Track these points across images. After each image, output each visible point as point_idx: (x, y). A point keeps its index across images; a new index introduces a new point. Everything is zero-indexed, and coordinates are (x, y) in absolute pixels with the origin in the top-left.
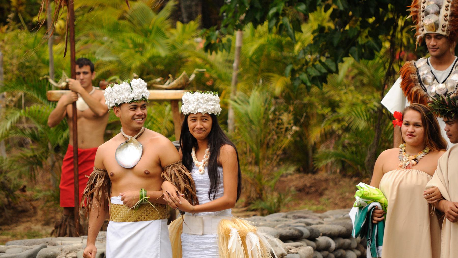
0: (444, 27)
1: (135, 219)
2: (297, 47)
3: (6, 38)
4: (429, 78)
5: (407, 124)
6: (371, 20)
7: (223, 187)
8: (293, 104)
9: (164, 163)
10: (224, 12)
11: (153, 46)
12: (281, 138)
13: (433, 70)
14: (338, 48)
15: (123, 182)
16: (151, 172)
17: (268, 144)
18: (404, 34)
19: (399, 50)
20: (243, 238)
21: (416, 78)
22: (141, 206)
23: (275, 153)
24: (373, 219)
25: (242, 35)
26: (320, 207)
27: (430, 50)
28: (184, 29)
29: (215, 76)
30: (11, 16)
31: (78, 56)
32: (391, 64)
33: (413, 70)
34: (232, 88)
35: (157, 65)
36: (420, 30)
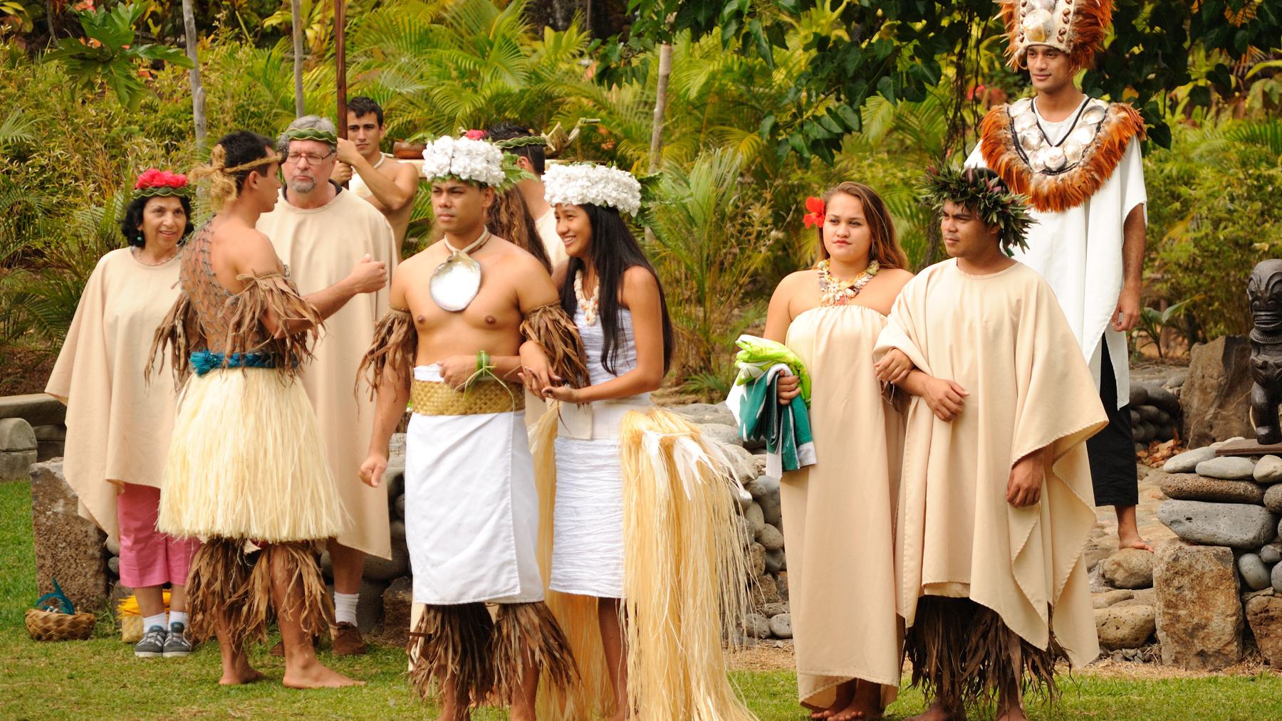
0: (1062, 34)
1: (462, 409)
2: (779, 76)
3: (210, 58)
4: (1033, 137)
5: (836, 221)
6: (919, 26)
7: (634, 348)
8: (772, 185)
9: (527, 305)
10: (636, 9)
11: (495, 74)
12: (748, 252)
13: (1041, 121)
14: (855, 78)
15: (438, 338)
16: (499, 319)
17: (722, 263)
18: (983, 52)
19: (973, 83)
20: (667, 449)
21: (1010, 136)
22: (478, 384)
23: (736, 282)
24: (779, 397)
25: (671, 55)
26: (244, 328)
27: (1034, 79)
28: (558, 42)
29: (617, 131)
30: (222, 15)
31: (352, 93)
32: (958, 109)
33: (1005, 121)
34: (651, 154)
35: (506, 110)
36: (1017, 39)
